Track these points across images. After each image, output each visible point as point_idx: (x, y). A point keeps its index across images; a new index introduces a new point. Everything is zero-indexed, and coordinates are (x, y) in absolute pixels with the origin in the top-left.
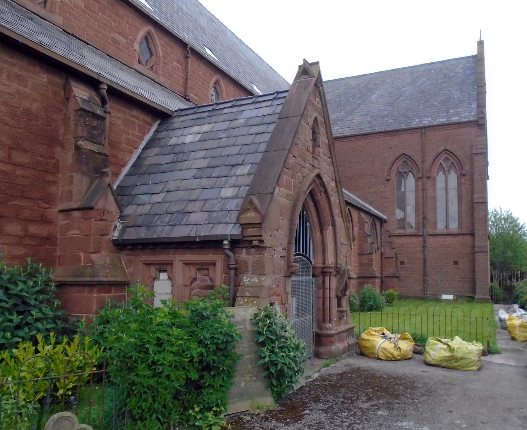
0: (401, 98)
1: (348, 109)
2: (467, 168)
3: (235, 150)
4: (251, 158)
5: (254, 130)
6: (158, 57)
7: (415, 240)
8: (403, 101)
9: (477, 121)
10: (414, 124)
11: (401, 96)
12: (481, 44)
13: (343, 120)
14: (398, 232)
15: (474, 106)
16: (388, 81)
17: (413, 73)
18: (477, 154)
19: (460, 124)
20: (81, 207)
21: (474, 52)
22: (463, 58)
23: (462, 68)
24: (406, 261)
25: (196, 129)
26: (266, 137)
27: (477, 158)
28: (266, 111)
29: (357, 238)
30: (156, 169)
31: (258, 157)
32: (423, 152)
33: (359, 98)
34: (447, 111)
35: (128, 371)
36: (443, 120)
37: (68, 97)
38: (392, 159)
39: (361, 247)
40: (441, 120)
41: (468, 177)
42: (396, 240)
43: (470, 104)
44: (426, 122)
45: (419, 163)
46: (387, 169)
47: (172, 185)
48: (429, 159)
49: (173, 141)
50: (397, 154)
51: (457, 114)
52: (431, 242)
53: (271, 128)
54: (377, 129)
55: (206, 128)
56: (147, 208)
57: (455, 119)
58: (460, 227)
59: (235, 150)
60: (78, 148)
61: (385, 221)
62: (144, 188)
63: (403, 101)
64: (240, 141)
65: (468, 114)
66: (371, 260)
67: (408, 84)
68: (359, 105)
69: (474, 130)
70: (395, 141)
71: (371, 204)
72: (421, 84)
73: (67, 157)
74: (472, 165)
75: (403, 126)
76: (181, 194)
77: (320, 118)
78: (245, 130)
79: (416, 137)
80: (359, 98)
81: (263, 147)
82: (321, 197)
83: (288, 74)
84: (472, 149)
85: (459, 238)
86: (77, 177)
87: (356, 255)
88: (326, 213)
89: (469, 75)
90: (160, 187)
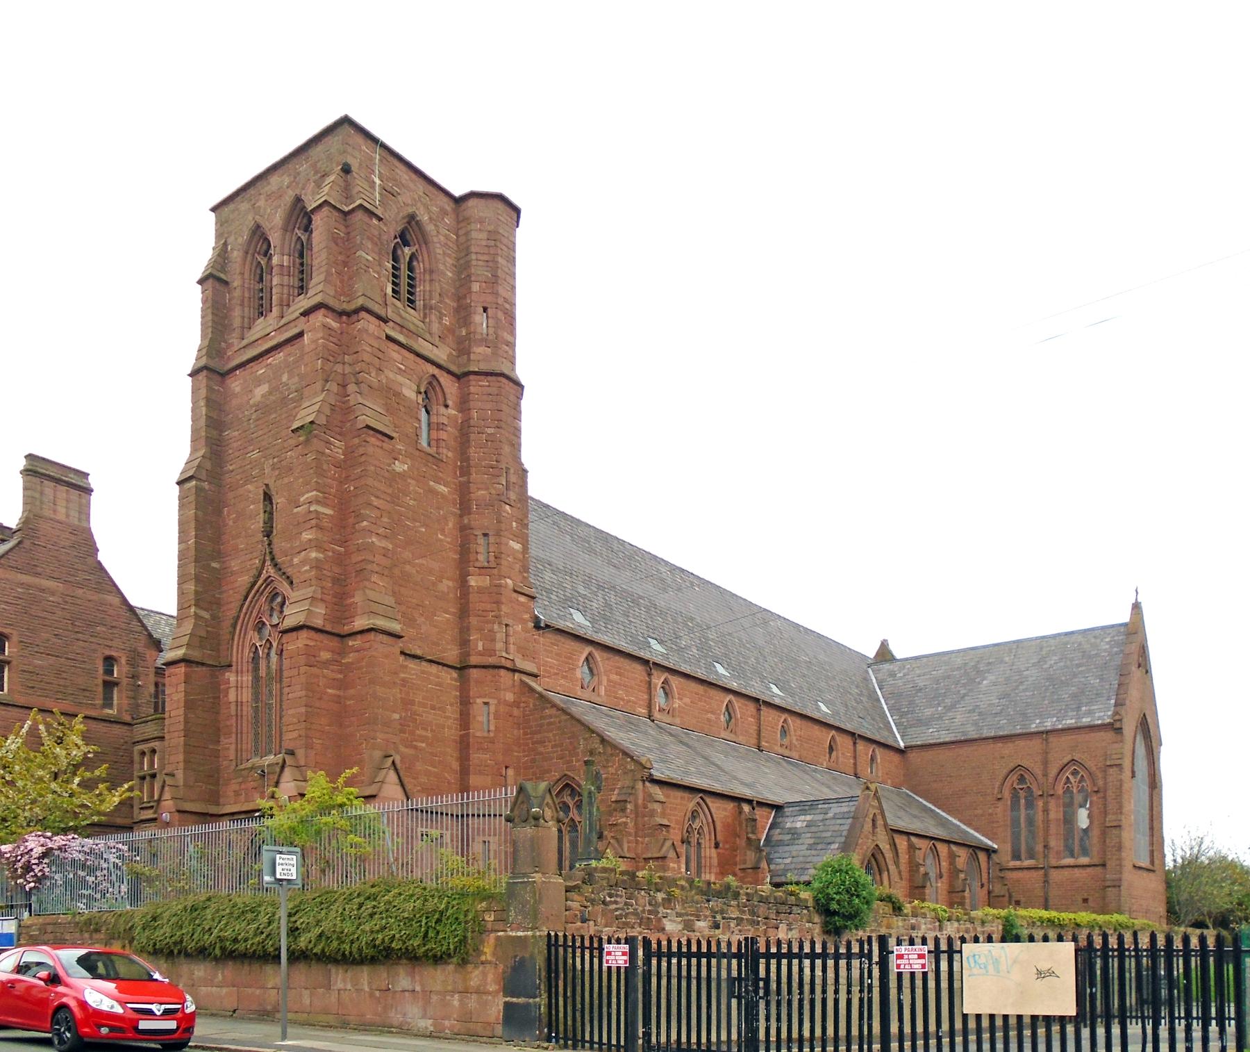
2: (1100, 783)
3: (829, 834)
4: (838, 840)
5: (839, 821)
6: (736, 719)
7: (1034, 874)
8: (1024, 690)
9: (1110, 724)
10: (1033, 727)
12: (1137, 607)
13: (940, 718)
14: (1013, 864)
16: (1007, 659)
17: (1041, 649)
19: (1092, 728)
21: (1125, 617)
22: (1113, 626)
23: (1108, 643)
24: (1023, 900)
25: (802, 818)
26: (846, 827)
28: (845, 809)
29: (945, 875)
30: (780, 843)
31: (843, 839)
32: (1045, 763)
33: (964, 685)
34: (1079, 708)
36: (1070, 722)
37: (741, 812)
38: (1005, 771)
39: (951, 885)
40: (1069, 722)
41: (1101, 795)
42: (1009, 875)
44: (1048, 724)
45: (1040, 777)
46: (997, 784)
47: (794, 854)
48: (1053, 772)
49: (788, 825)
50: (1012, 765)
51: (1090, 713)
52: (1055, 875)
53: (850, 821)
54: (987, 733)
55: (808, 818)
56: (782, 867)
57: (1086, 720)
59: (829, 834)
60: (748, 838)
61: (995, 851)
62: (777, 855)
63: (1024, 690)
64: (832, 828)
66: (964, 897)
67: (1034, 665)
68: (965, 695)
69: (1109, 736)
70: (1007, 749)
71: (976, 830)
72: (1051, 666)
73: (743, 843)
74: (1105, 778)
75: (1018, 730)
76: (801, 859)
77: (877, 811)
78: (833, 822)
79: (1036, 744)
80: (964, 685)
81: (845, 833)
82: (879, 857)
83: (871, 652)
85: (1089, 870)
86: (748, 853)
87: (945, 892)
88: (883, 863)
90: (787, 855)
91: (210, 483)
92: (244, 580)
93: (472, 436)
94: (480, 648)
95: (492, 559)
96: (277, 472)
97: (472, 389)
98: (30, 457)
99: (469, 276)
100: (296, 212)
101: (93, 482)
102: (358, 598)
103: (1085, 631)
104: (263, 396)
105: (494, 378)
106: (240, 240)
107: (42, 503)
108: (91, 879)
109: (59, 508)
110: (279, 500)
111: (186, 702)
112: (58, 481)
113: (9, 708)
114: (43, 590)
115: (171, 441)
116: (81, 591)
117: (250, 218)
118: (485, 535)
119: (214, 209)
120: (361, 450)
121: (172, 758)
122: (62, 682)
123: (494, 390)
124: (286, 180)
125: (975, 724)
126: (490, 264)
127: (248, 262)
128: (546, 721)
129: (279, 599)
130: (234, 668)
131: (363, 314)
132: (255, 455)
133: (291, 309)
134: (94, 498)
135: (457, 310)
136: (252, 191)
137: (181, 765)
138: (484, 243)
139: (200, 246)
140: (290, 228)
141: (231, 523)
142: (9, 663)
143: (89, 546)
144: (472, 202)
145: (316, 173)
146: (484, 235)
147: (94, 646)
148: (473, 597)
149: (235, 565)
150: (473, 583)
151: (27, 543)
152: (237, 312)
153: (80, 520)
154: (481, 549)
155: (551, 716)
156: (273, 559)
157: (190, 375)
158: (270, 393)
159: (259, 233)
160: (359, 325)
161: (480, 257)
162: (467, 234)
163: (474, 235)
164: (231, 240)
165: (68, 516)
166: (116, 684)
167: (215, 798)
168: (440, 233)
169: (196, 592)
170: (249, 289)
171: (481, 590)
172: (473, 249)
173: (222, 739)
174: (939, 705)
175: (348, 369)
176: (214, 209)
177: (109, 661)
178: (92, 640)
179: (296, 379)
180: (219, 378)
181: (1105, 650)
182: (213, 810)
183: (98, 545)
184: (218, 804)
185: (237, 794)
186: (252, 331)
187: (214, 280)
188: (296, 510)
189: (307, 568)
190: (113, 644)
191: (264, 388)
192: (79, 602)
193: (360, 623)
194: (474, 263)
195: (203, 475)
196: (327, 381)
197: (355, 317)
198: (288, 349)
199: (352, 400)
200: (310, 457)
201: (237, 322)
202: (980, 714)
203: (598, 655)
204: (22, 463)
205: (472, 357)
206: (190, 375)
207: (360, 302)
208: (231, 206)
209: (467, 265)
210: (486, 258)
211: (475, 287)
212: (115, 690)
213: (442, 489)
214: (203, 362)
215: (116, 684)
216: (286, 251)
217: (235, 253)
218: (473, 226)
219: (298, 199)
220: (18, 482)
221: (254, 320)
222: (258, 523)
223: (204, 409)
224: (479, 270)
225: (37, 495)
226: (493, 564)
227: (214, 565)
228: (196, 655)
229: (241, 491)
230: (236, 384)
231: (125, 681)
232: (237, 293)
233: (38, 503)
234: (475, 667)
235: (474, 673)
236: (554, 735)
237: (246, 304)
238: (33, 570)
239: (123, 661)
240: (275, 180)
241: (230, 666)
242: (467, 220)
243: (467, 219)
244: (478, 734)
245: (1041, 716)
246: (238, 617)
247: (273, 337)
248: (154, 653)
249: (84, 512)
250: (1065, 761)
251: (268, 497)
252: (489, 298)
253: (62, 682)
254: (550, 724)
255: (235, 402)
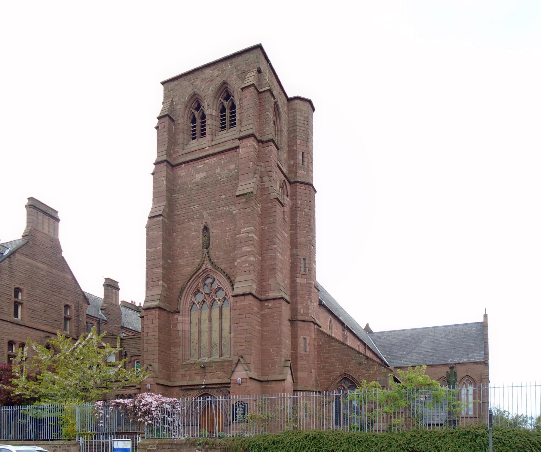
0: (440, 346)
1: (408, 350)
8: (442, 347)
11: (440, 344)
12: (485, 316)
15: (483, 353)
18: (484, 378)
20: (86, 294)
21: (482, 320)
22: (475, 323)
23: (475, 330)
27: (484, 380)
33: (414, 344)
34: (468, 355)
35: (21, 348)
36: (465, 360)
43: (480, 352)
58: (475, 413)
63: (442, 347)
65: (479, 358)
69: (483, 366)
80: (414, 344)
83: (363, 326)
84: (481, 375)
89: (480, 331)
91: (168, 220)
92: (188, 270)
93: (298, 212)
94: (302, 312)
95: (307, 271)
96: (213, 217)
97: (298, 190)
98: (31, 199)
99: (296, 136)
100: (223, 88)
101: (120, 285)
102: (271, 282)
103: (464, 324)
104: (201, 179)
105: (308, 186)
106: (183, 100)
107: (37, 223)
108: (170, 419)
109: (45, 227)
110: (214, 231)
111: (159, 328)
112: (45, 213)
113: (23, 327)
114: (38, 268)
115: (139, 199)
116: (55, 271)
117: (190, 89)
118: (304, 259)
119: (163, 83)
120: (273, 210)
121: (149, 357)
122: (46, 316)
123: (307, 192)
124: (216, 73)
125: (422, 359)
126: (305, 132)
127: (187, 111)
128: (332, 348)
129: (209, 281)
130: (181, 313)
131: (272, 143)
132: (196, 207)
133: (218, 137)
134: (60, 224)
135: (289, 151)
136: (191, 76)
137: (157, 361)
138: (303, 122)
139: (155, 103)
140: (217, 97)
141: (178, 240)
142: (21, 304)
143: (56, 248)
144: (297, 101)
145: (238, 71)
146: (302, 118)
147: (61, 299)
148: (299, 288)
149: (181, 262)
150: (298, 281)
151: (31, 243)
152: (181, 136)
153: (54, 234)
154: (302, 265)
155: (335, 346)
156: (210, 260)
157: (154, 164)
158: (207, 177)
159: (194, 98)
160: (269, 148)
161: (301, 128)
162: (294, 116)
163: (298, 117)
164: (175, 99)
165: (49, 232)
166: (70, 319)
167: (169, 378)
168: (283, 109)
169: (163, 273)
170: (187, 125)
171: (302, 285)
172: (298, 124)
173: (172, 348)
174: (404, 351)
175: (263, 170)
176: (163, 83)
177: (67, 307)
178: (60, 295)
179: (226, 171)
180: (170, 167)
181: (474, 333)
182: (170, 384)
183: (62, 249)
184: (170, 381)
185: (183, 376)
186: (189, 146)
187: (167, 118)
188: (238, 236)
189: (247, 265)
190: (69, 298)
191: (203, 175)
192: (54, 276)
193: (271, 295)
194: (298, 130)
195: (165, 215)
196: (255, 174)
197: (266, 144)
198: (220, 156)
199: (267, 184)
200: (248, 210)
201: (180, 141)
202: (424, 355)
203: (333, 320)
204: (26, 202)
205: (298, 175)
206: (154, 164)
207: (270, 137)
208: (176, 82)
209: (295, 131)
210: (303, 129)
211: (299, 142)
212: (68, 323)
213: (286, 235)
214: (164, 158)
215: (70, 319)
216: (215, 108)
217: (179, 107)
218: (298, 113)
219: (225, 83)
220: (25, 212)
221: (189, 141)
222: (198, 242)
223: (165, 182)
224: (300, 133)
225: (35, 219)
226: (307, 273)
227: (169, 261)
228: (162, 305)
229: (186, 225)
230: (182, 172)
231: (73, 318)
232: (181, 126)
233: (36, 223)
234: (300, 321)
235: (300, 324)
236: (337, 355)
237: (185, 132)
238: (33, 256)
239: (73, 308)
240: (208, 72)
241: (179, 312)
242: (295, 110)
243: (294, 109)
244: (301, 353)
245: (452, 358)
246: (185, 288)
247: (208, 150)
248: (86, 305)
249: (56, 230)
250: (464, 375)
251: (206, 229)
252: (305, 149)
253: (46, 316)
254: (335, 349)
255: (180, 181)
